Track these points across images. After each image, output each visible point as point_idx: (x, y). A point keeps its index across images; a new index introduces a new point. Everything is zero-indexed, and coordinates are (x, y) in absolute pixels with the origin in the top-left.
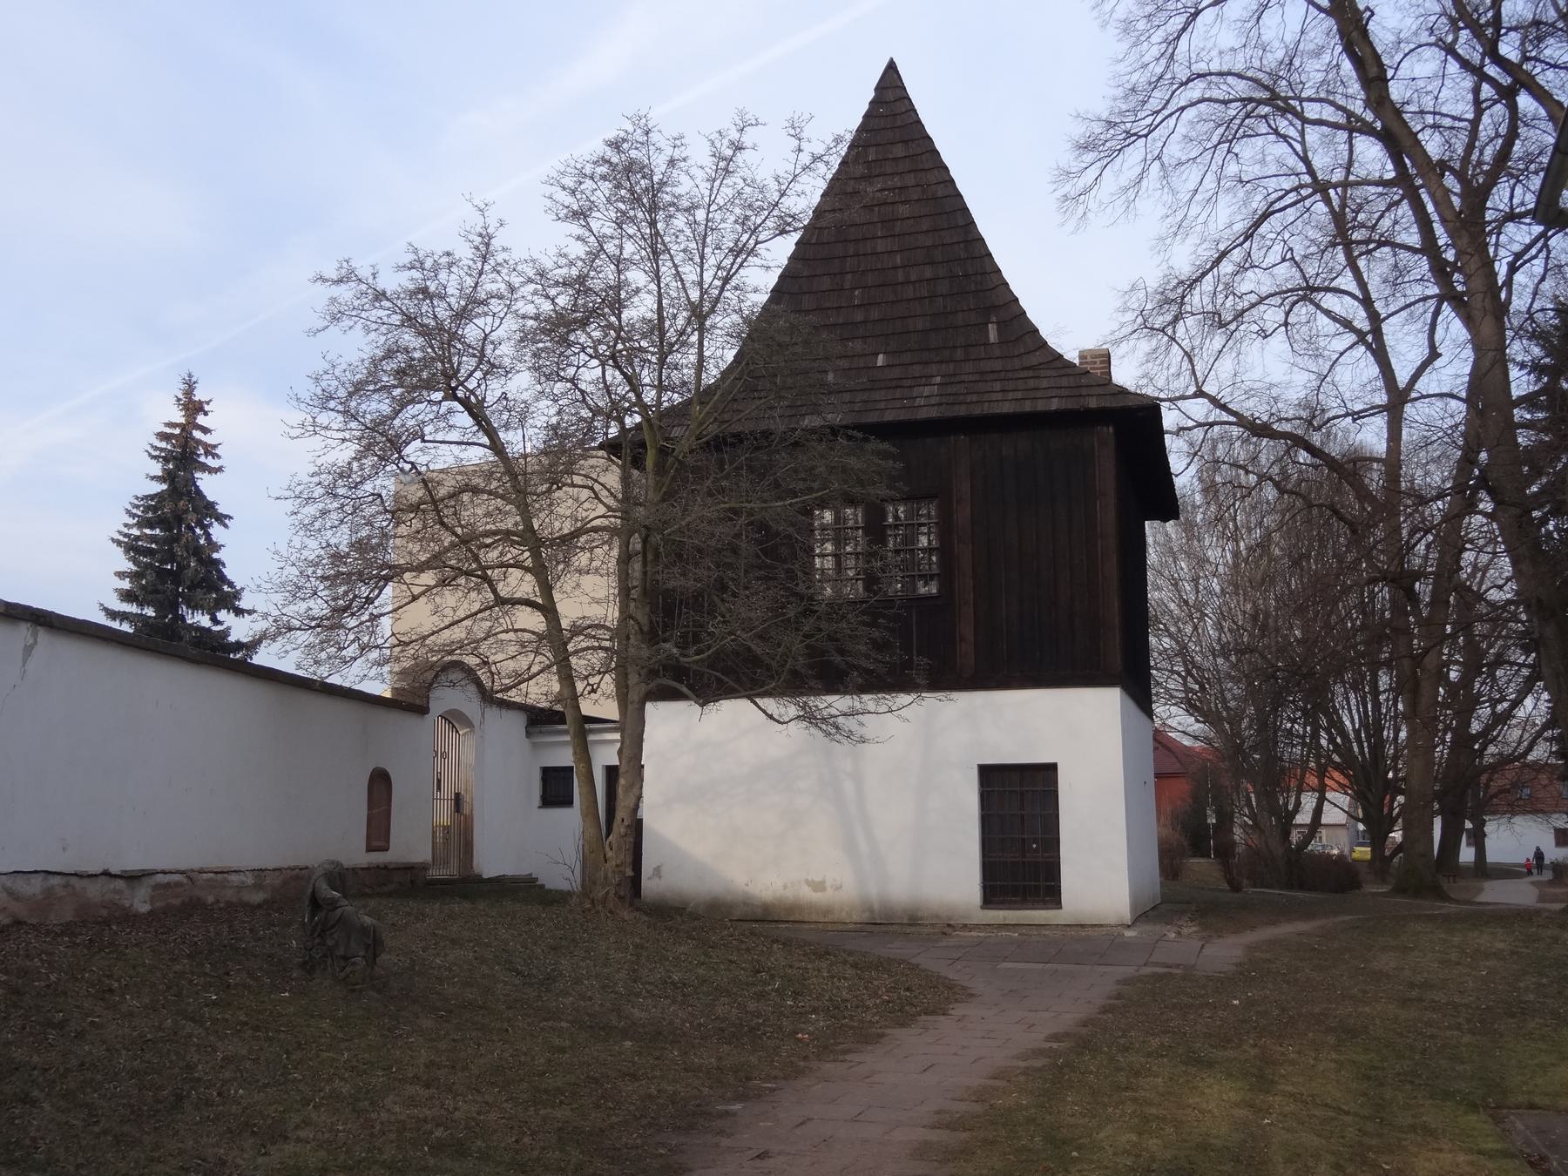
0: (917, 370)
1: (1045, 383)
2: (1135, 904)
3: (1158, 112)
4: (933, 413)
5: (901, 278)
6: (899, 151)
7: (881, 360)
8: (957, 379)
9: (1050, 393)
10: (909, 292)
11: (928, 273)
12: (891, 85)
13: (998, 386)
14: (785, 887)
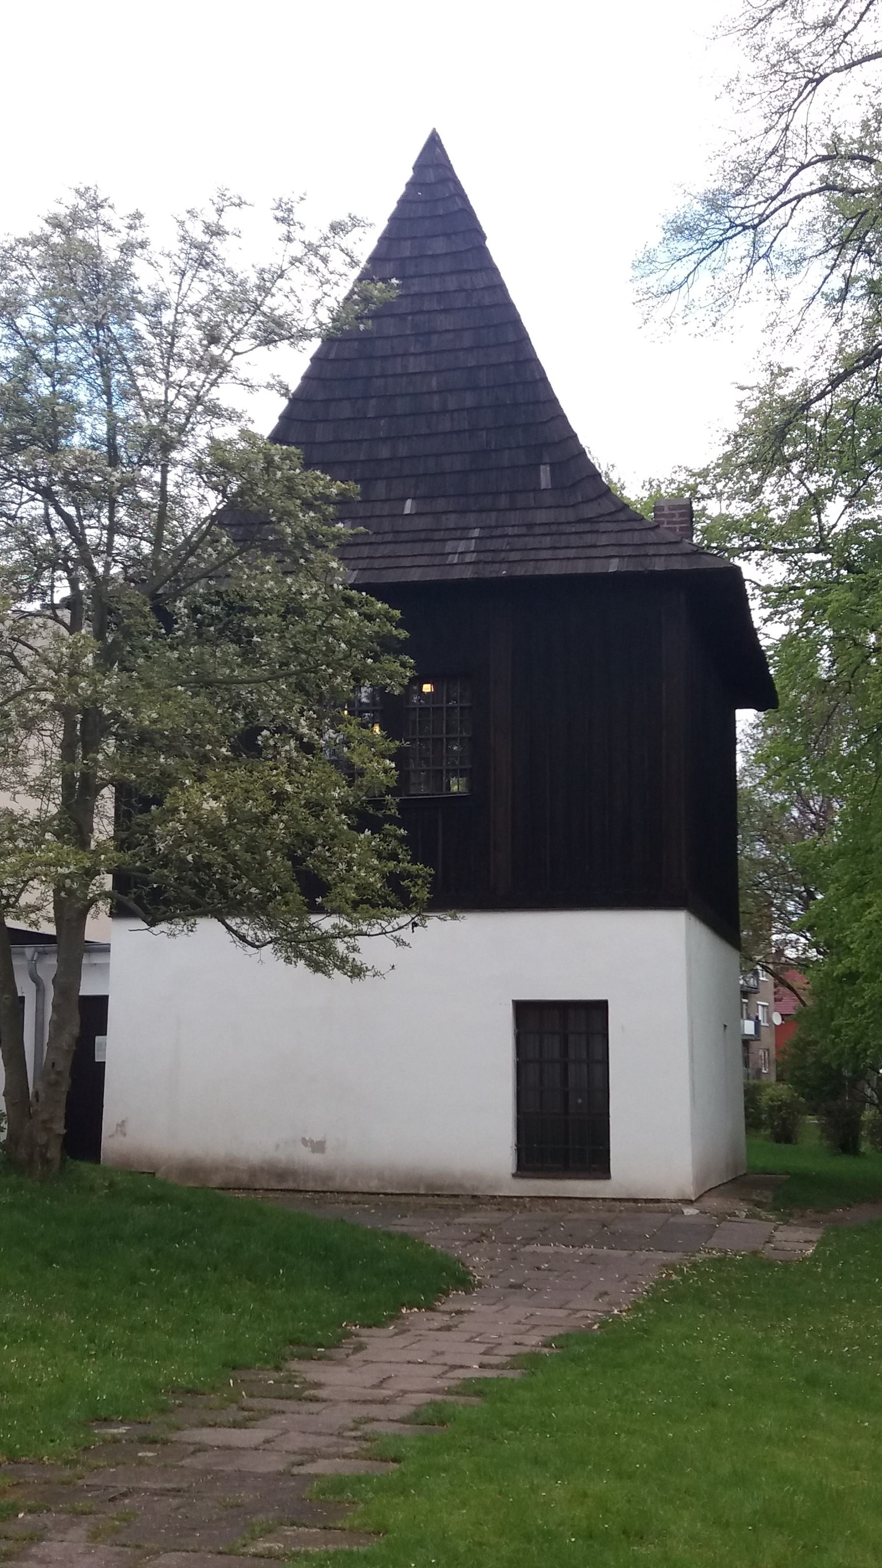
0: (451, 521)
1: (604, 540)
2: (698, 1180)
3: (773, 199)
4: (468, 573)
5: (436, 406)
6: (439, 246)
7: (409, 507)
8: (499, 532)
9: (610, 551)
10: (446, 425)
11: (469, 400)
12: (433, 164)
13: (547, 541)
14: (278, 1146)
